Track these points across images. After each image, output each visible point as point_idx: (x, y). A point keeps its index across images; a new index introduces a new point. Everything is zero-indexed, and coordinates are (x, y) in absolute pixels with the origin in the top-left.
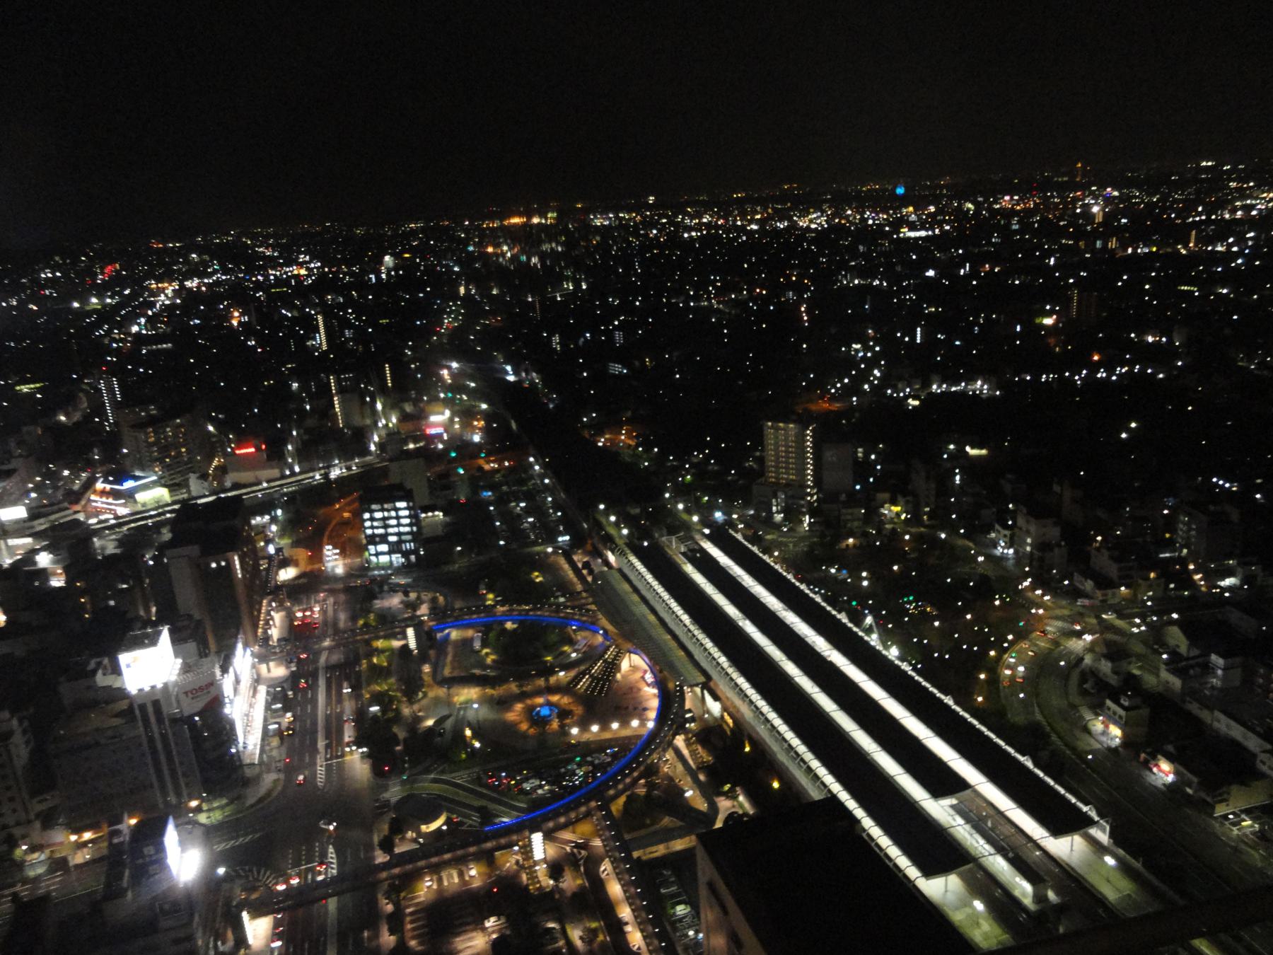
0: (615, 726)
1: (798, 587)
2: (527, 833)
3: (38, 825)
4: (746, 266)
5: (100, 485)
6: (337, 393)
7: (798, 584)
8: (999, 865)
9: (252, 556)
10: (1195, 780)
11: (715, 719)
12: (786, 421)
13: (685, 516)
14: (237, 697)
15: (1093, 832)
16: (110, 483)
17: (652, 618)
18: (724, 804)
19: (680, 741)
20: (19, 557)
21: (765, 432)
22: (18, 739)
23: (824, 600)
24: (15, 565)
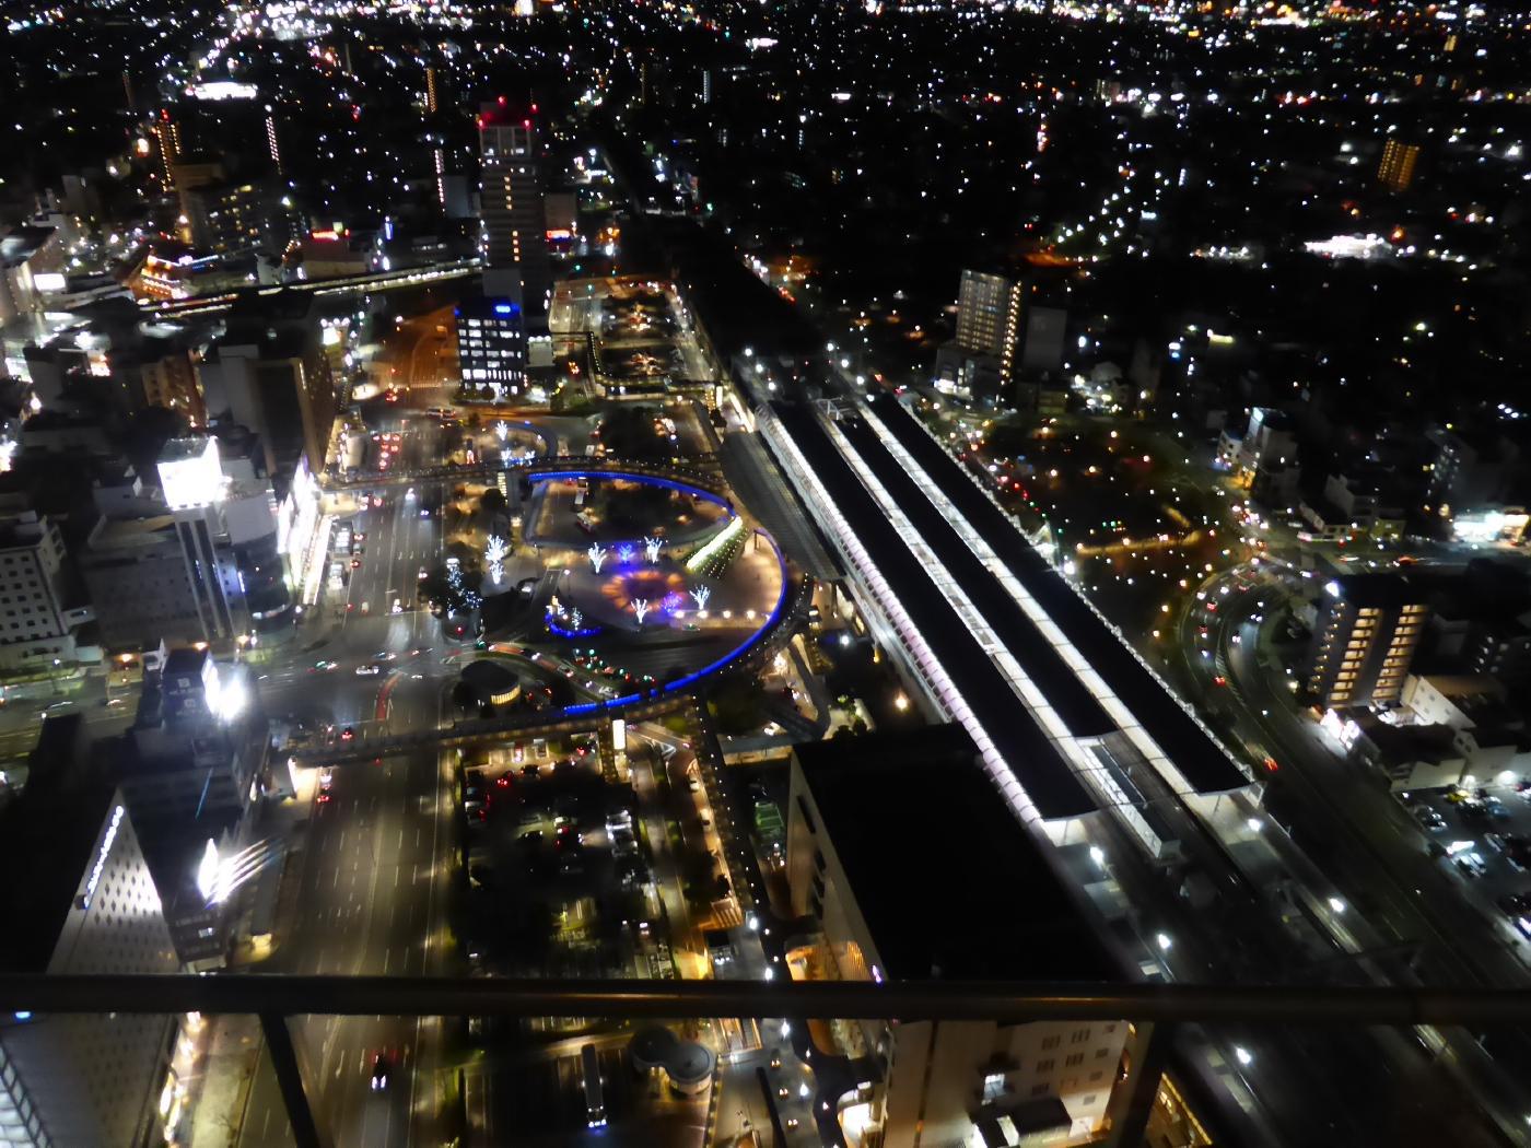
0: (727, 614)
1: (969, 479)
2: (608, 719)
3: (71, 640)
4: (980, 60)
5: (152, 260)
6: (445, 174)
7: (969, 475)
8: (1130, 814)
9: (340, 373)
10: (1377, 751)
11: (845, 620)
12: (991, 272)
13: (847, 377)
14: (295, 529)
15: (1246, 792)
16: (1082, 591)
17: (788, 495)
18: (838, 717)
19: (798, 639)
20: (57, 335)
21: (962, 283)
22: (46, 543)
23: (997, 499)
24: (51, 347)
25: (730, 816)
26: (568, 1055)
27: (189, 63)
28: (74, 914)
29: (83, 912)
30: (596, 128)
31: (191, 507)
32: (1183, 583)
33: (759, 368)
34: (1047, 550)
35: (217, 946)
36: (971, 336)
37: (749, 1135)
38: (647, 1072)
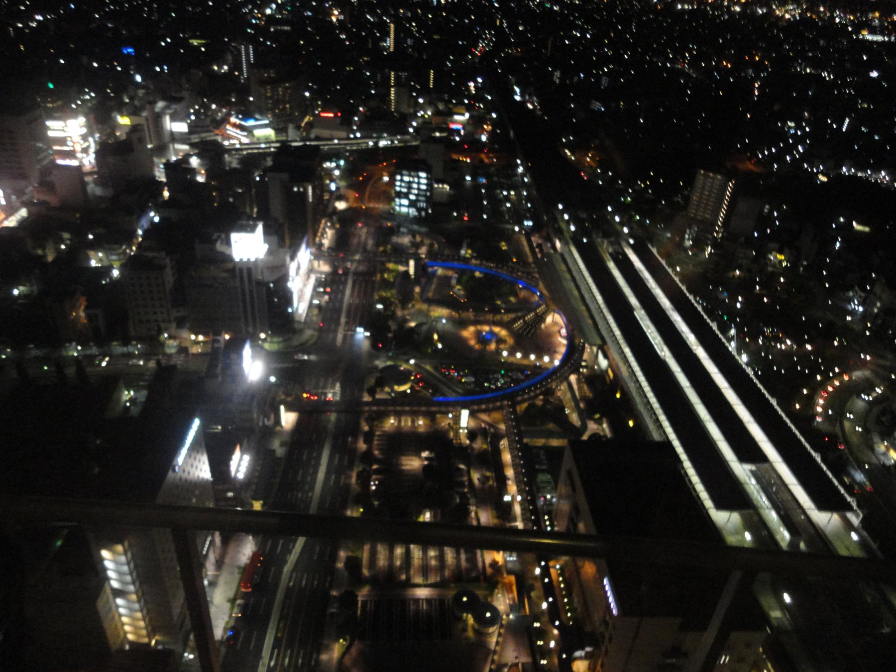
5: (233, 120)
8: (772, 516)
15: (851, 516)
17: (576, 293)
18: (592, 426)
19: (573, 378)
22: (169, 271)
25: (524, 475)
26: (417, 597)
27: (261, 11)
28: (170, 474)
29: (175, 474)
30: (484, 66)
31: (245, 260)
32: (819, 378)
33: (566, 217)
34: (732, 346)
35: (234, 503)
36: (707, 200)
37: (517, 665)
38: (462, 617)
